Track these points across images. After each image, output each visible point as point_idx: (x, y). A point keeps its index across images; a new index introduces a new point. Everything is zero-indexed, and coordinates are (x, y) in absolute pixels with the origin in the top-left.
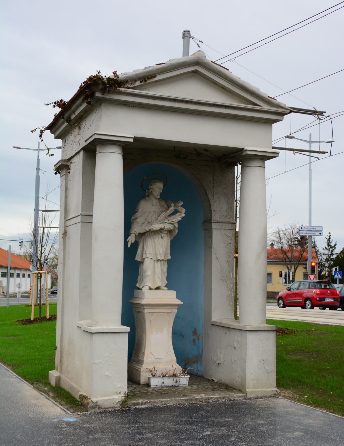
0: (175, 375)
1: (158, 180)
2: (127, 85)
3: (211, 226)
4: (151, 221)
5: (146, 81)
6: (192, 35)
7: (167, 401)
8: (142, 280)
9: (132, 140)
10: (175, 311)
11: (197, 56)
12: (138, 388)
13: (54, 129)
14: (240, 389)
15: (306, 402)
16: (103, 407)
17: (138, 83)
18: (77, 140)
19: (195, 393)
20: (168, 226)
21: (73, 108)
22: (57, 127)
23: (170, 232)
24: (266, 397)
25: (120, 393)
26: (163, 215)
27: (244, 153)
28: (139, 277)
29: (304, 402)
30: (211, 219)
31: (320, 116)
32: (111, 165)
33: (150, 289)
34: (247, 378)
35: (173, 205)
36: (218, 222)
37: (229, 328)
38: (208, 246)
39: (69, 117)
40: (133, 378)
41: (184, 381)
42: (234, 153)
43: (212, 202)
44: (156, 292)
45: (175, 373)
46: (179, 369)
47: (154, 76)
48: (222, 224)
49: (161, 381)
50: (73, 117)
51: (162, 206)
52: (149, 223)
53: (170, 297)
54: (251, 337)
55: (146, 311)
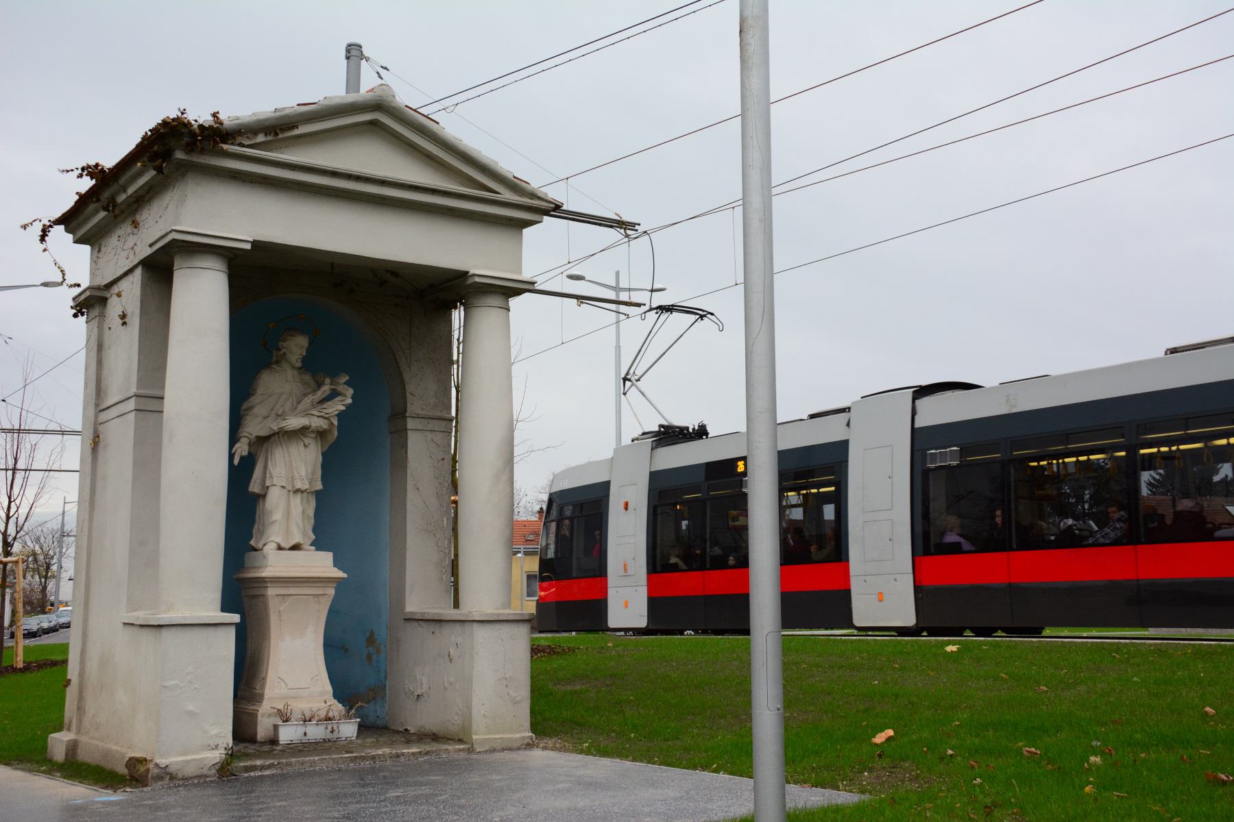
0: (328, 719)
1: (296, 330)
2: (239, 140)
3: (406, 425)
4: (284, 412)
5: (277, 134)
6: (366, 53)
7: (314, 762)
8: (262, 533)
9: (248, 247)
10: (332, 592)
11: (379, 93)
12: (256, 747)
13: (74, 224)
14: (461, 737)
15: (588, 752)
16: (180, 776)
17: (261, 138)
18: (130, 244)
19: (370, 747)
20: (317, 423)
21: (122, 180)
22: (81, 218)
23: (321, 434)
24: (510, 749)
25: (217, 746)
26: (308, 401)
27: (470, 281)
28: (256, 526)
29: (581, 752)
30: (405, 411)
31: (629, 232)
32: (202, 298)
33: (280, 548)
34: (474, 712)
35: (328, 381)
36: (418, 417)
37: (440, 621)
38: (399, 463)
39: (112, 200)
40: (243, 730)
41: (349, 730)
42: (449, 281)
43: (407, 377)
44: (290, 553)
45: (330, 715)
46: (338, 708)
47: (293, 126)
48: (426, 421)
49: (301, 730)
50: (121, 198)
51: (305, 384)
52: (278, 416)
53: (322, 564)
54: (481, 633)
55: (271, 592)
